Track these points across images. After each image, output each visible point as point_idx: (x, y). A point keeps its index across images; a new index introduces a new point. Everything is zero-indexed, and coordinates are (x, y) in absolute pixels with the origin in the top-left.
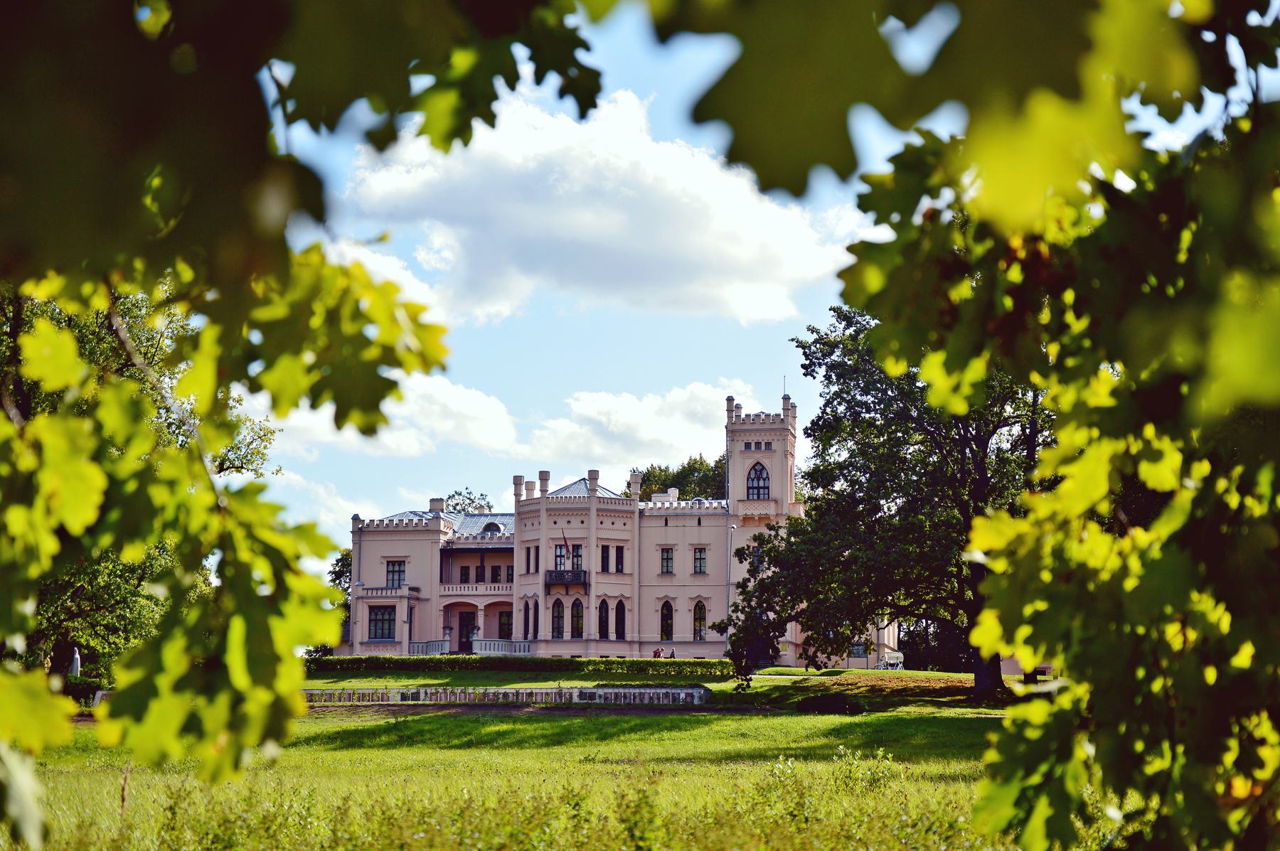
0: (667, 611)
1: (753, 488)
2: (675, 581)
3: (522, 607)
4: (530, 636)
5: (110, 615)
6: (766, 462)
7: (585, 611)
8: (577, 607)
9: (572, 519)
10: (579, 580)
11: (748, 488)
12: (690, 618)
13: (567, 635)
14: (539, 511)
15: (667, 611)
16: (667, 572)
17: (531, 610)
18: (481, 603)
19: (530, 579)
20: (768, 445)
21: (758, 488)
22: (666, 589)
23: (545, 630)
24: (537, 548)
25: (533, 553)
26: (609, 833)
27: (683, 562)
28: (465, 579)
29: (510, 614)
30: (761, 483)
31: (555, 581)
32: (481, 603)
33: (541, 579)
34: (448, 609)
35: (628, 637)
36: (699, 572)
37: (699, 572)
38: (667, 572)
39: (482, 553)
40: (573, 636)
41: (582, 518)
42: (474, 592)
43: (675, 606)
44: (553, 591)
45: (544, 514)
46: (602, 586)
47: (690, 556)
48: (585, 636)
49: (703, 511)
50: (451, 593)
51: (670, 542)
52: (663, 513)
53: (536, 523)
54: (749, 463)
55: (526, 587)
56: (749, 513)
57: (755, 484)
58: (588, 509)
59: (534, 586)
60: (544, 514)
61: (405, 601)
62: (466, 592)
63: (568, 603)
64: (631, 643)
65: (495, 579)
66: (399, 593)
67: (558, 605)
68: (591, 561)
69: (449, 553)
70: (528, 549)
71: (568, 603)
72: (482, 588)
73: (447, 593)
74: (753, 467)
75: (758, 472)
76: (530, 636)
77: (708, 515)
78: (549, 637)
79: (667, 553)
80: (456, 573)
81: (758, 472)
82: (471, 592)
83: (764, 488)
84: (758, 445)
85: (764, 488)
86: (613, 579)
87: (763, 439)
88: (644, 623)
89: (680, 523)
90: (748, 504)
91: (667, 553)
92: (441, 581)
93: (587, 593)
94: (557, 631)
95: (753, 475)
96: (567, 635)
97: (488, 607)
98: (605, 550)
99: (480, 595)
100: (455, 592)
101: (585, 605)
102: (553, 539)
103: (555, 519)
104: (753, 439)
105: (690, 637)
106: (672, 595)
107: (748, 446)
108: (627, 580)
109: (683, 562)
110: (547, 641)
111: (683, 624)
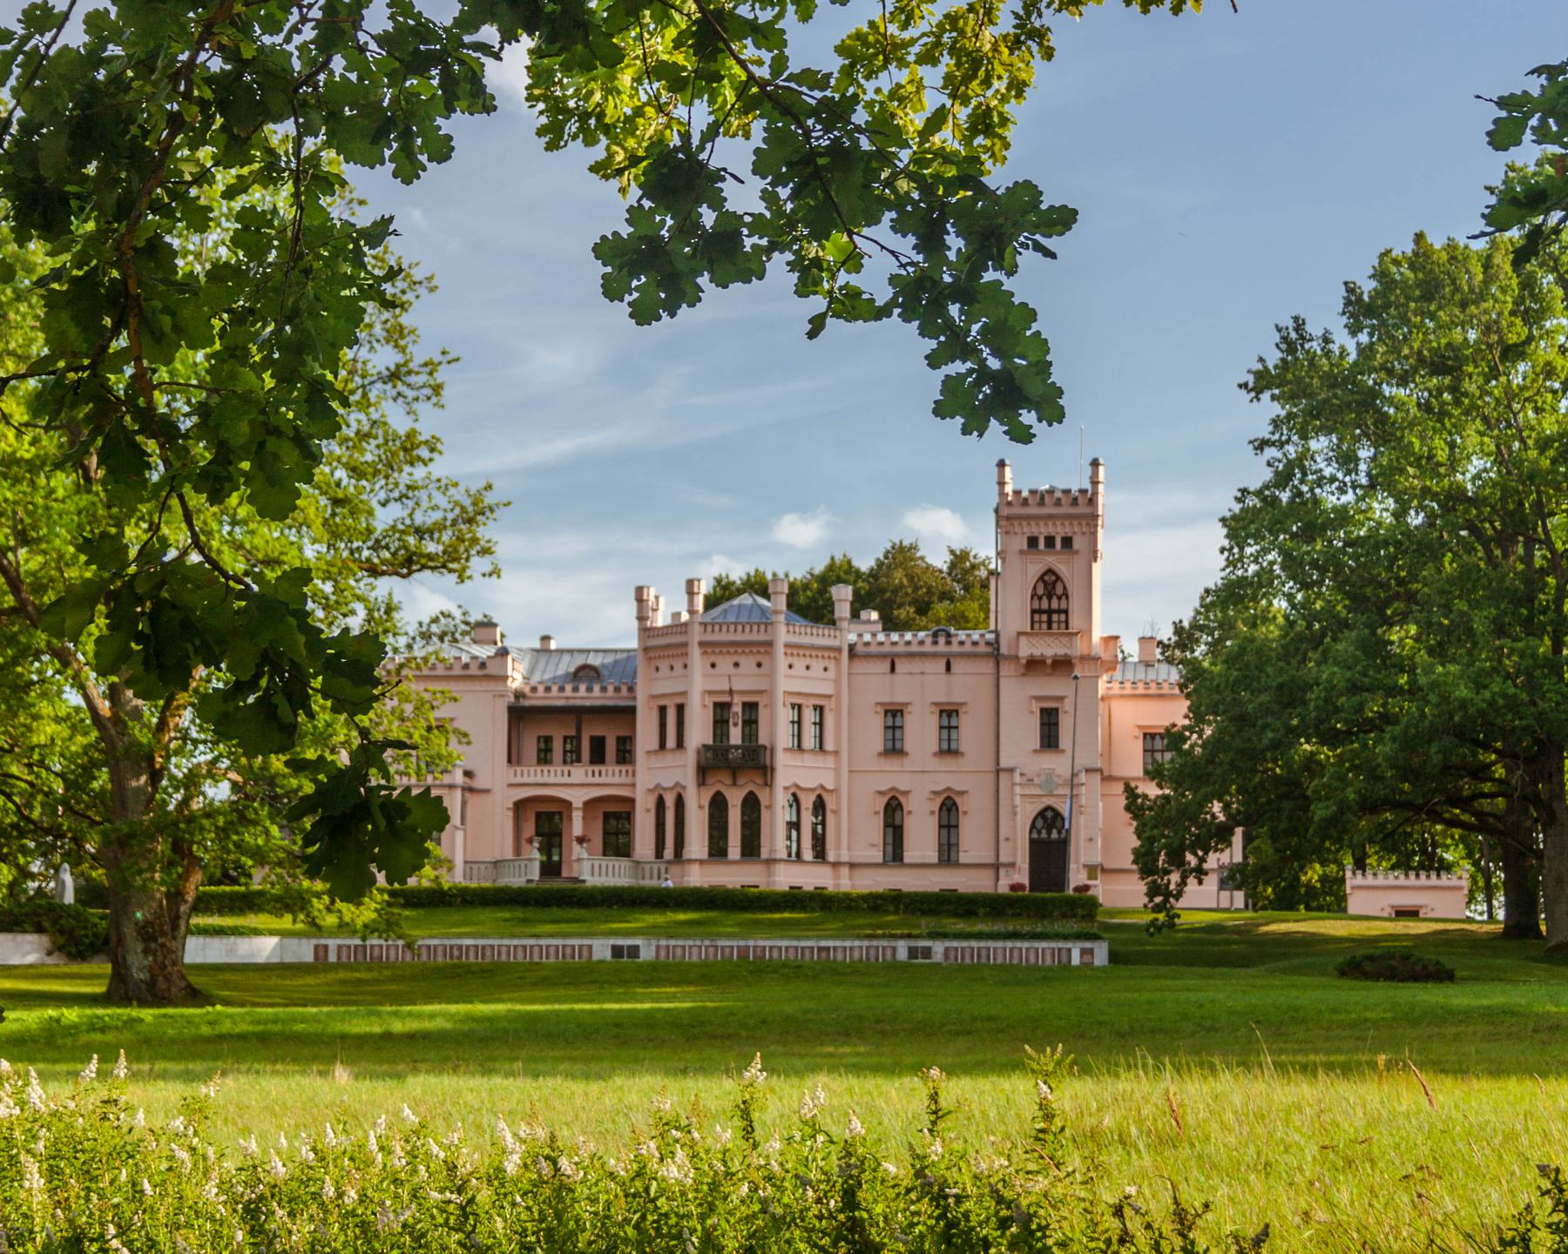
0: (893, 810)
1: (1040, 611)
2: (907, 764)
3: (652, 805)
4: (669, 853)
5: (225, 795)
6: (1062, 569)
7: (765, 814)
8: (752, 806)
9: (742, 660)
10: (754, 761)
11: (1033, 612)
12: (932, 824)
13: (734, 851)
14: (685, 645)
15: (893, 810)
16: (894, 749)
17: (670, 810)
18: (577, 798)
19: (669, 759)
20: (1067, 542)
21: (1050, 612)
22: (893, 776)
23: (697, 845)
24: (680, 709)
25: (673, 715)
26: (820, 1181)
27: (921, 732)
28: (544, 757)
29: (629, 816)
30: (1055, 605)
31: (715, 761)
32: (577, 798)
33: (690, 759)
34: (520, 806)
35: (831, 857)
36: (948, 751)
37: (948, 751)
38: (894, 749)
39: (578, 714)
40: (743, 854)
41: (759, 658)
42: (566, 780)
43: (909, 804)
44: (710, 781)
45: (695, 652)
46: (794, 771)
47: (932, 722)
48: (764, 854)
49: (955, 648)
50: (526, 780)
51: (899, 699)
52: (887, 649)
53: (678, 665)
54: (1035, 569)
55: (659, 772)
56: (1037, 652)
57: (1045, 605)
58: (685, 645)
59: (678, 771)
60: (695, 652)
61: (458, 793)
62: (552, 780)
63: (735, 799)
64: (836, 865)
65: (598, 757)
66: (446, 779)
67: (718, 806)
68: (778, 729)
69: (521, 715)
70: (663, 710)
71: (735, 799)
72: (579, 773)
73: (519, 780)
74: (1041, 578)
75: (1050, 584)
76: (669, 853)
77: (911, 655)
78: (705, 856)
79: (894, 715)
80: (530, 747)
81: (1050, 584)
82: (560, 780)
83: (1059, 611)
84: (1050, 541)
85: (1059, 611)
86: (809, 760)
87: (1059, 531)
88: (856, 835)
89: (916, 666)
90: (1033, 640)
91: (894, 715)
92: (509, 761)
93: (769, 783)
94: (718, 850)
95: (1040, 591)
96: (734, 851)
97: (590, 805)
98: (663, 710)
99: (575, 784)
100: (532, 780)
101: (764, 801)
102: (711, 693)
103: (713, 659)
104: (1042, 531)
105: (932, 856)
106: (903, 787)
107: (1033, 542)
108: (830, 762)
109: (921, 732)
110: (701, 862)
111: (921, 839)
